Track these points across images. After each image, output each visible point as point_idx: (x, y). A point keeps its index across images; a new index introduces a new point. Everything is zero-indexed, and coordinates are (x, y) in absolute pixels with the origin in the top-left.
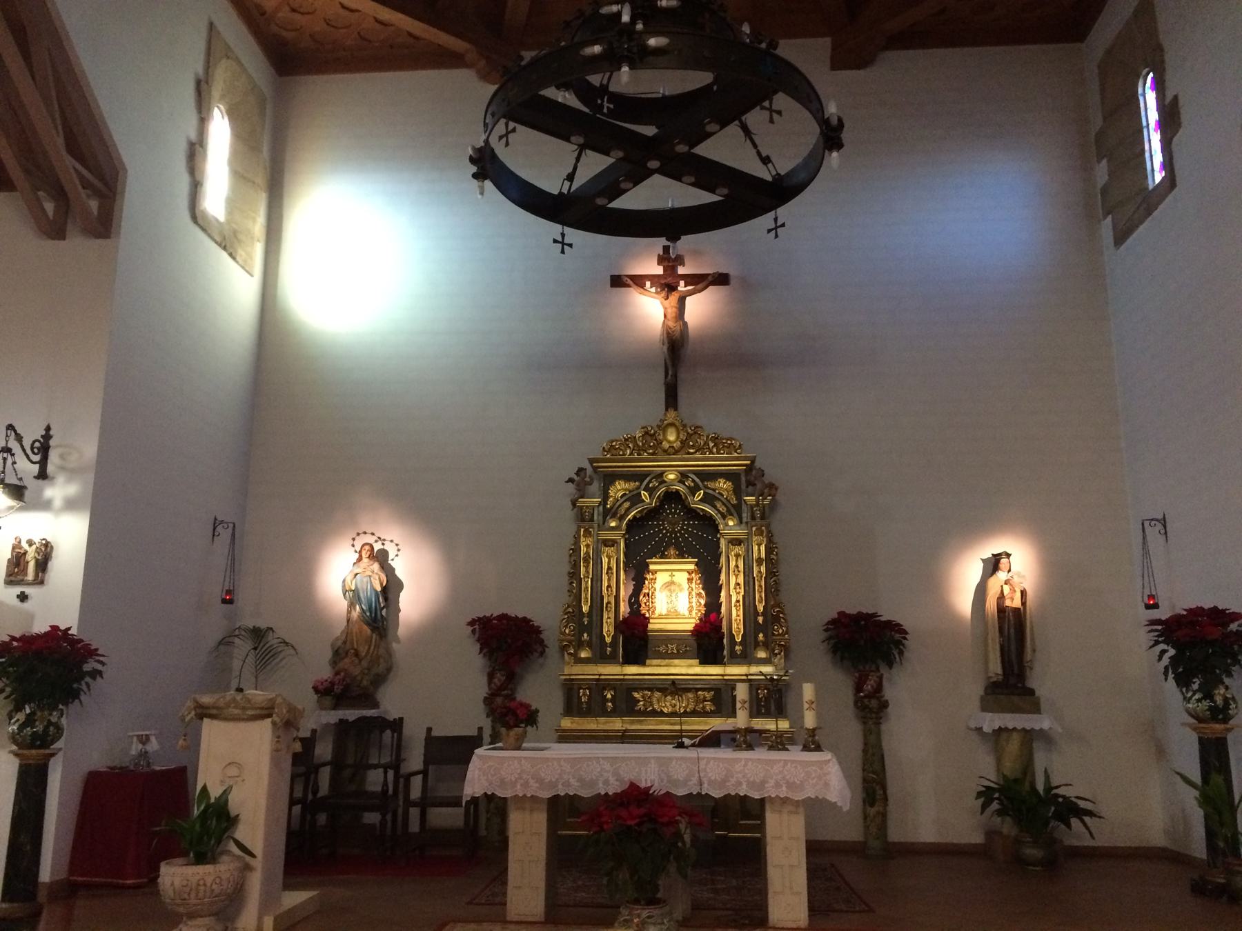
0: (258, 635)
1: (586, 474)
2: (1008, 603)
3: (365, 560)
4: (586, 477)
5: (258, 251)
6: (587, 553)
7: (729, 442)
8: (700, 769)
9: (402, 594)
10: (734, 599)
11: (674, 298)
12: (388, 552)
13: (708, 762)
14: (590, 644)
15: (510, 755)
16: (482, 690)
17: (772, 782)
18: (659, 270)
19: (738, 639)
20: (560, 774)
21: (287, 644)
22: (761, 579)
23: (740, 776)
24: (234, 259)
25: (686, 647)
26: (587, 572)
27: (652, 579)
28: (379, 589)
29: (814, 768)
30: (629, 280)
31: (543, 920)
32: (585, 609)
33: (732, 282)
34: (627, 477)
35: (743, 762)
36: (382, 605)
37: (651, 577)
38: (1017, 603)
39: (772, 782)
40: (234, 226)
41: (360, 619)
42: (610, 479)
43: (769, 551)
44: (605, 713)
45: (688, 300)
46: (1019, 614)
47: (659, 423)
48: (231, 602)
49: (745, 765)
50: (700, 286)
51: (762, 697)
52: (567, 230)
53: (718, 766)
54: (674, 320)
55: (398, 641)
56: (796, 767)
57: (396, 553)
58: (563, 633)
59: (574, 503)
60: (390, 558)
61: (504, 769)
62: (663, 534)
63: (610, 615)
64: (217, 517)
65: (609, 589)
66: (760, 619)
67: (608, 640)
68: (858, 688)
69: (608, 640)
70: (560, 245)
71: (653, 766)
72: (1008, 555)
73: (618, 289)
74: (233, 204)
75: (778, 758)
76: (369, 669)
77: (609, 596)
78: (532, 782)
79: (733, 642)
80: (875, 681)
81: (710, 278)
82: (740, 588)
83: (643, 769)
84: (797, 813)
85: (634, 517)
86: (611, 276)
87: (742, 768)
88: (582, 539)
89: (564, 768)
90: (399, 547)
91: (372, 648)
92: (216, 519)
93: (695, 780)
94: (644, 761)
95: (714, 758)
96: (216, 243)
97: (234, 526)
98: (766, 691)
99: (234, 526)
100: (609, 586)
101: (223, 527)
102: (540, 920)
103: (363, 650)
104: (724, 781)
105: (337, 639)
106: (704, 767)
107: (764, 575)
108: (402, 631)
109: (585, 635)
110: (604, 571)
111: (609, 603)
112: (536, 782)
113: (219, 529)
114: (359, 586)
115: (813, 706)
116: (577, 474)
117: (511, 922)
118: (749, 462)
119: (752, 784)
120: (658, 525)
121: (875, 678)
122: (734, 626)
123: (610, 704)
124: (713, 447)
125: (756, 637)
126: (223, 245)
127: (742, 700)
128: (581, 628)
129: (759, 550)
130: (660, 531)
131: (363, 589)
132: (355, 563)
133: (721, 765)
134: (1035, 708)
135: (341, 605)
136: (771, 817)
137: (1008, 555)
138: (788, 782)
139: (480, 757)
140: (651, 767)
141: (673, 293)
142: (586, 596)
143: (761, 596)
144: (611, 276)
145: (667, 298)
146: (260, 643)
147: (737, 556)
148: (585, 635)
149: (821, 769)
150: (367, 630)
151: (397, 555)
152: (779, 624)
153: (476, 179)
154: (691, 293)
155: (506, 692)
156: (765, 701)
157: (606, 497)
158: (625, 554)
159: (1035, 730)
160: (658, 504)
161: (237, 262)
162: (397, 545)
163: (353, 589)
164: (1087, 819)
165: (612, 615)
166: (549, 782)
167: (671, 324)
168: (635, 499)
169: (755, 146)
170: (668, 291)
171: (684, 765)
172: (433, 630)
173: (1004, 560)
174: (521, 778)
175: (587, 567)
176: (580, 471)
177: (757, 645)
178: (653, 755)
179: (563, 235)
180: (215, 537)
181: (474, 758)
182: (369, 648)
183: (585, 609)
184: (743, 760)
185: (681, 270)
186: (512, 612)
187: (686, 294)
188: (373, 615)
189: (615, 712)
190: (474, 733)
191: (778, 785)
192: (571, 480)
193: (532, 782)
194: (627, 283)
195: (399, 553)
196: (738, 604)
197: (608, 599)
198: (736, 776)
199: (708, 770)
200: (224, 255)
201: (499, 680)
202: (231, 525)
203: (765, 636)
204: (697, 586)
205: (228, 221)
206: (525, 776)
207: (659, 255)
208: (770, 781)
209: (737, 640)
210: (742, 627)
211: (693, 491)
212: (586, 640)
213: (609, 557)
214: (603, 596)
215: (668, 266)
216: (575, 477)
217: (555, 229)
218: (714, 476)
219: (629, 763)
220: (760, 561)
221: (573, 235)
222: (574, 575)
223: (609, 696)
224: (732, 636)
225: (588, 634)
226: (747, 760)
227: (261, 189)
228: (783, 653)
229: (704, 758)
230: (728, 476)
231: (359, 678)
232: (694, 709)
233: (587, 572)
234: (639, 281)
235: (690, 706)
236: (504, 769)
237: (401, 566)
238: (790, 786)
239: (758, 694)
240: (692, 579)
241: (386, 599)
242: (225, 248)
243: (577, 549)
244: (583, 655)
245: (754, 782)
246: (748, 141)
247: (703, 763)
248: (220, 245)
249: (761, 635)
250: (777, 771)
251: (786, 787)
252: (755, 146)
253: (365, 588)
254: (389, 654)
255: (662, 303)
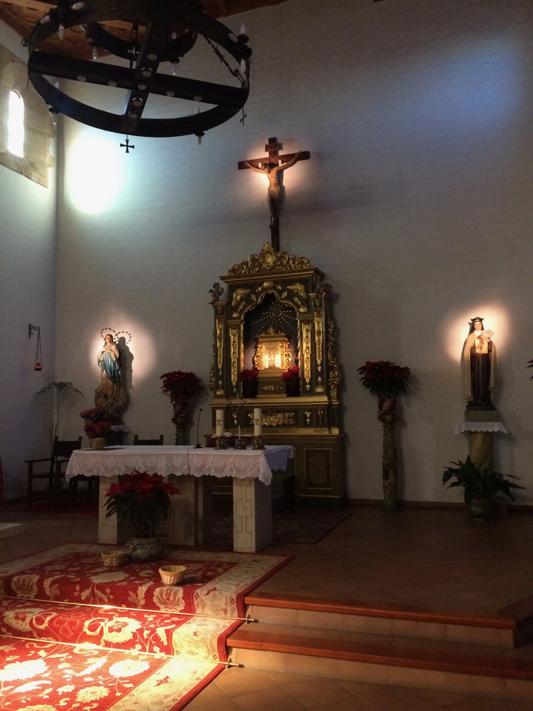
0: (61, 386)
1: (219, 286)
2: (478, 351)
3: (109, 344)
4: (219, 289)
5: (50, 173)
6: (220, 334)
7: (302, 260)
8: (189, 461)
9: (133, 362)
10: (305, 357)
11: (274, 171)
12: (124, 338)
13: (193, 457)
14: (322, 384)
15: (89, 453)
16: (172, 414)
17: (228, 468)
18: (266, 155)
19: (308, 381)
20: (116, 464)
21: (78, 391)
22: (320, 344)
23: (211, 464)
24: (30, 178)
25: (279, 386)
26: (221, 345)
27: (260, 347)
28: (114, 360)
29: (251, 459)
30: (248, 163)
31: (115, 542)
32: (220, 366)
33: (312, 156)
34: (243, 287)
35: (212, 457)
36: (117, 368)
37: (260, 346)
38: (485, 350)
39: (228, 468)
40: (32, 160)
41: (106, 376)
42: (233, 288)
43: (327, 326)
44: (306, 426)
45: (285, 172)
46: (487, 357)
47: (261, 252)
48: (40, 370)
49: (214, 458)
50: (290, 162)
51: (320, 415)
52: (130, 137)
53: (199, 459)
54: (274, 186)
55: (131, 387)
56: (241, 460)
57: (129, 339)
58: (211, 381)
59: (212, 303)
60: (126, 342)
61: (88, 461)
62: (284, 318)
63: (235, 370)
64: (31, 324)
65: (234, 354)
66: (319, 368)
67: (234, 384)
68: (380, 406)
69: (234, 384)
70: (126, 147)
71: (164, 459)
72: (481, 320)
73: (244, 170)
74: (28, 147)
75: (233, 454)
76: (112, 404)
77: (234, 358)
78: (101, 468)
79: (305, 383)
80: (389, 404)
81: (296, 156)
82: (309, 350)
83: (159, 461)
84: (250, 486)
85: (248, 311)
86: (238, 162)
87: (211, 460)
88: (217, 325)
89: (118, 461)
90: (131, 336)
91: (115, 392)
92: (30, 325)
93: (186, 467)
94: (158, 456)
95: (196, 454)
96: (15, 171)
97: (39, 328)
98: (322, 412)
99: (39, 328)
100: (234, 352)
101: (34, 329)
102: (114, 544)
103: (109, 393)
104: (203, 467)
105: (99, 388)
106: (191, 459)
107: (322, 342)
108: (134, 383)
109: (220, 382)
110: (232, 344)
111: (234, 362)
112: (124, 468)
113: (32, 331)
114: (104, 358)
115: (258, 422)
116: (214, 287)
117: (101, 544)
118: (313, 272)
119: (216, 469)
120: (268, 314)
121: (389, 401)
122: (306, 373)
123: (236, 421)
124: (292, 264)
125: (317, 379)
126: (20, 171)
127: (257, 419)
128: (218, 378)
129: (318, 326)
130: (269, 317)
131: (106, 360)
132: (104, 346)
133: (221, 459)
134: (498, 418)
135: (98, 369)
136: (236, 489)
137: (481, 320)
138: (236, 468)
139: (76, 454)
140: (163, 460)
141: (274, 169)
142: (220, 359)
143: (319, 355)
144: (238, 162)
145: (270, 172)
146: (62, 390)
147: (307, 331)
148: (220, 382)
149: (256, 460)
150: (110, 382)
151: (130, 340)
152: (333, 371)
153: (51, 112)
154: (286, 167)
155: (182, 415)
156: (322, 418)
157: (230, 298)
158: (244, 333)
159: (495, 432)
160: (261, 302)
161: (33, 180)
162: (130, 334)
163: (102, 360)
164: (511, 490)
165: (236, 370)
166: (131, 467)
167: (273, 188)
168: (246, 299)
169: (227, 65)
170: (269, 168)
171: (221, 459)
172: (147, 382)
173: (477, 323)
174: (96, 466)
175: (220, 342)
176: (216, 285)
177: (317, 384)
178: (163, 453)
179: (127, 141)
180: (31, 336)
181: (73, 455)
182: (113, 392)
183: (220, 366)
184: (212, 455)
185: (281, 153)
186: (184, 370)
187: (283, 168)
188: (113, 374)
189: (310, 425)
190: (77, 440)
191: (231, 470)
192: (211, 291)
193: (101, 468)
194: (247, 165)
195: (131, 339)
196: (307, 360)
197: (234, 360)
198: (209, 464)
199: (193, 461)
200: (23, 177)
201: (178, 409)
202: (37, 328)
203: (322, 379)
204: (286, 350)
205: (26, 157)
206: (119, 465)
207: (266, 145)
208: (227, 467)
209: (307, 382)
210: (310, 373)
211: (280, 292)
212: (220, 385)
213: (234, 336)
214: (231, 359)
215: (272, 151)
216: (214, 289)
217: (121, 138)
218: (292, 282)
219: (111, 458)
220: (319, 332)
221: (133, 140)
222: (215, 346)
223: (308, 416)
224: (304, 379)
225: (221, 381)
226: (236, 456)
227: (49, 136)
228: (336, 388)
229: (191, 454)
230: (302, 281)
231: (106, 409)
232: (283, 423)
233: (221, 345)
234: (253, 164)
235: (280, 421)
236: (88, 461)
237: (132, 346)
238: (239, 470)
239: (317, 413)
240: (283, 346)
241: (120, 365)
242: (21, 173)
243: (215, 331)
244: (219, 393)
245: (197, 468)
246: (223, 62)
247: (190, 457)
248: (17, 172)
249: (320, 378)
250: (231, 462)
251: (236, 471)
252: (227, 65)
253: (107, 359)
254: (127, 396)
255: (267, 175)
